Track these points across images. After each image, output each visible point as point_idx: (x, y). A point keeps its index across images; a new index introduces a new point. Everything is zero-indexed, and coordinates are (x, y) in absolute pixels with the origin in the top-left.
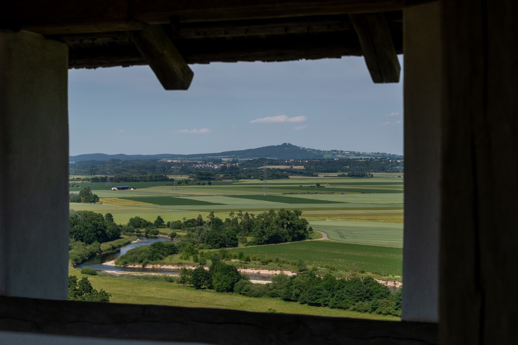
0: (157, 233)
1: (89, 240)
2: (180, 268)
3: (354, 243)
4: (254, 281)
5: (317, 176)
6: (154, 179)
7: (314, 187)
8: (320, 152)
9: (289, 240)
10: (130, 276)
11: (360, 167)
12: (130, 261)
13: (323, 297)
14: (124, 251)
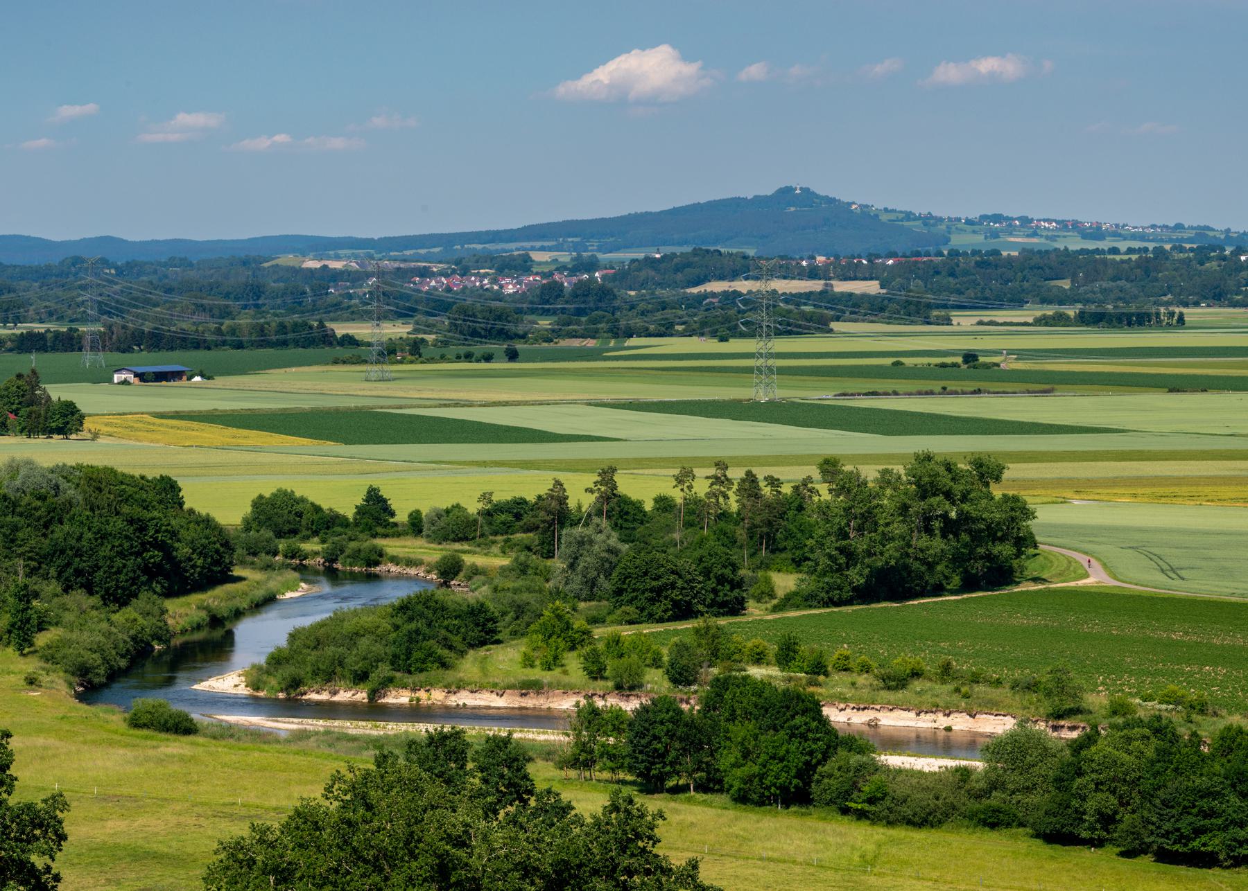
0: (376, 557)
1: (117, 587)
3: (1233, 599)
4: (894, 761)
5: (948, 321)
6: (274, 338)
7: (955, 365)
8: (934, 225)
9: (949, 587)
10: (338, 739)
11: (1118, 282)
12: (315, 673)
13: (1228, 825)
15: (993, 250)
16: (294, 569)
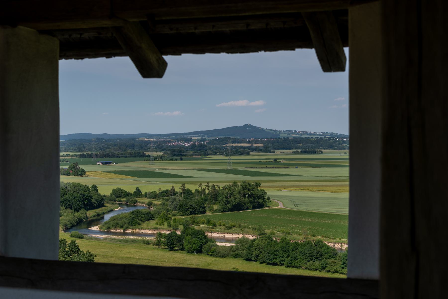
0: (136, 202)
1: (77, 208)
2: (156, 232)
3: (306, 211)
4: (219, 244)
5: (275, 153)
6: (133, 155)
7: (272, 162)
8: (277, 132)
9: (250, 208)
10: (113, 240)
11: (311, 144)
12: (113, 226)
13: (279, 257)
14: (107, 217)
15: (327, 132)
16: (118, 204)
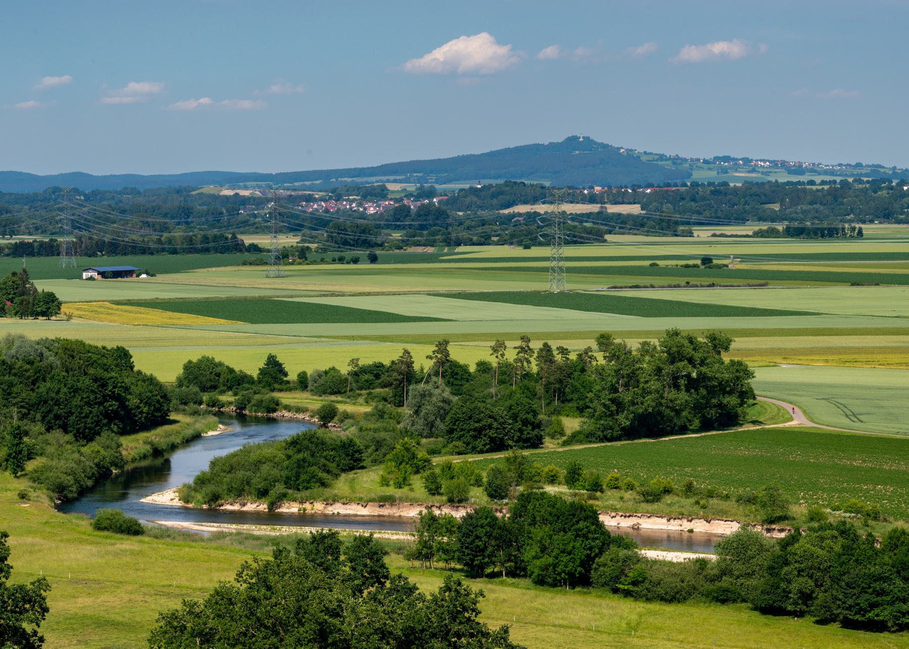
0: (274, 406)
1: (85, 428)
3: (898, 437)
4: (651, 554)
5: (691, 234)
6: (199, 246)
7: (695, 266)
8: (681, 164)
9: (691, 428)
10: (246, 538)
11: (815, 206)
12: (230, 490)
13: (894, 601)
